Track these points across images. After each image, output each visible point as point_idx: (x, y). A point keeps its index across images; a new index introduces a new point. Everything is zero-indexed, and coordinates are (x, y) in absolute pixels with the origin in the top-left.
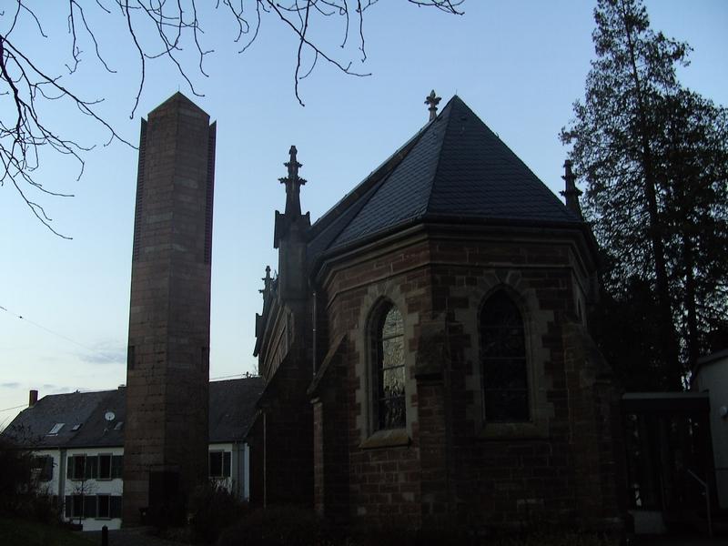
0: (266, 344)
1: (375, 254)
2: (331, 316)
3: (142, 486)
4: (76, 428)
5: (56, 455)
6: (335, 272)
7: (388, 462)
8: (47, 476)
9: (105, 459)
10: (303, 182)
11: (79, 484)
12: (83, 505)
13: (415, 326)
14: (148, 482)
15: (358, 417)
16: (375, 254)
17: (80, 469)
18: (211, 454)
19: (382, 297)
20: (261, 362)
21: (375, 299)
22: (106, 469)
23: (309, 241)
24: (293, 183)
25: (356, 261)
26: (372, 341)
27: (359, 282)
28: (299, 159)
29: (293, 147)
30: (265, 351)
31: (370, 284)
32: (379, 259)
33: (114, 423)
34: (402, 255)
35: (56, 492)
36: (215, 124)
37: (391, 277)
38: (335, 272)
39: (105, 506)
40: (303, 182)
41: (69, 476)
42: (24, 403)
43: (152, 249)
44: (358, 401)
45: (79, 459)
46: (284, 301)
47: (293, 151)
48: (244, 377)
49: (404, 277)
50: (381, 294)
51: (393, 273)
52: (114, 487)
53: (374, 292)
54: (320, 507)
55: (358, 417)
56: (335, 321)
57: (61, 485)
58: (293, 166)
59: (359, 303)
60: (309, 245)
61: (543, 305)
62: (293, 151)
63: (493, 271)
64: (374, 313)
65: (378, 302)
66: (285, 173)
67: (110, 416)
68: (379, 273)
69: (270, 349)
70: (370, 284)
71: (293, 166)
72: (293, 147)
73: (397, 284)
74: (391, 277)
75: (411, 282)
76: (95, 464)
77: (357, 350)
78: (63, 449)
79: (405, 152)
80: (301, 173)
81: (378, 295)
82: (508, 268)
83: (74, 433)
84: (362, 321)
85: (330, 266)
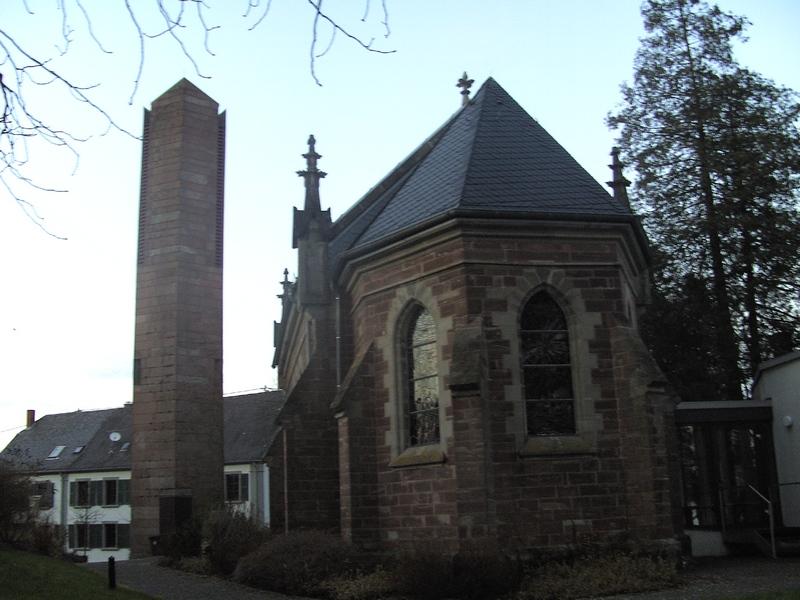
0: (285, 356)
3: (152, 512)
4: (78, 450)
5: (56, 480)
6: (360, 274)
8: (48, 504)
9: (111, 484)
10: (323, 175)
11: (83, 512)
12: (86, 535)
13: (449, 331)
15: (387, 432)
17: (83, 495)
19: (413, 300)
20: (280, 373)
21: (405, 302)
22: (112, 494)
23: (331, 240)
24: (312, 177)
29: (312, 136)
30: (284, 361)
33: (119, 444)
35: (57, 520)
36: (224, 113)
38: (360, 274)
39: (112, 535)
40: (323, 175)
41: (72, 503)
42: (22, 424)
43: (157, 252)
44: (387, 415)
45: (82, 484)
46: (305, 306)
47: (312, 141)
48: (263, 391)
49: (436, 277)
51: (424, 274)
52: (121, 514)
53: (403, 295)
56: (360, 328)
57: (62, 513)
58: (312, 157)
59: (386, 307)
60: (331, 244)
61: (591, 307)
62: (312, 141)
63: (534, 270)
66: (303, 166)
67: (115, 437)
71: (312, 157)
72: (312, 136)
78: (65, 473)
80: (321, 165)
81: (408, 298)
83: (76, 456)
84: (390, 327)
85: (354, 267)
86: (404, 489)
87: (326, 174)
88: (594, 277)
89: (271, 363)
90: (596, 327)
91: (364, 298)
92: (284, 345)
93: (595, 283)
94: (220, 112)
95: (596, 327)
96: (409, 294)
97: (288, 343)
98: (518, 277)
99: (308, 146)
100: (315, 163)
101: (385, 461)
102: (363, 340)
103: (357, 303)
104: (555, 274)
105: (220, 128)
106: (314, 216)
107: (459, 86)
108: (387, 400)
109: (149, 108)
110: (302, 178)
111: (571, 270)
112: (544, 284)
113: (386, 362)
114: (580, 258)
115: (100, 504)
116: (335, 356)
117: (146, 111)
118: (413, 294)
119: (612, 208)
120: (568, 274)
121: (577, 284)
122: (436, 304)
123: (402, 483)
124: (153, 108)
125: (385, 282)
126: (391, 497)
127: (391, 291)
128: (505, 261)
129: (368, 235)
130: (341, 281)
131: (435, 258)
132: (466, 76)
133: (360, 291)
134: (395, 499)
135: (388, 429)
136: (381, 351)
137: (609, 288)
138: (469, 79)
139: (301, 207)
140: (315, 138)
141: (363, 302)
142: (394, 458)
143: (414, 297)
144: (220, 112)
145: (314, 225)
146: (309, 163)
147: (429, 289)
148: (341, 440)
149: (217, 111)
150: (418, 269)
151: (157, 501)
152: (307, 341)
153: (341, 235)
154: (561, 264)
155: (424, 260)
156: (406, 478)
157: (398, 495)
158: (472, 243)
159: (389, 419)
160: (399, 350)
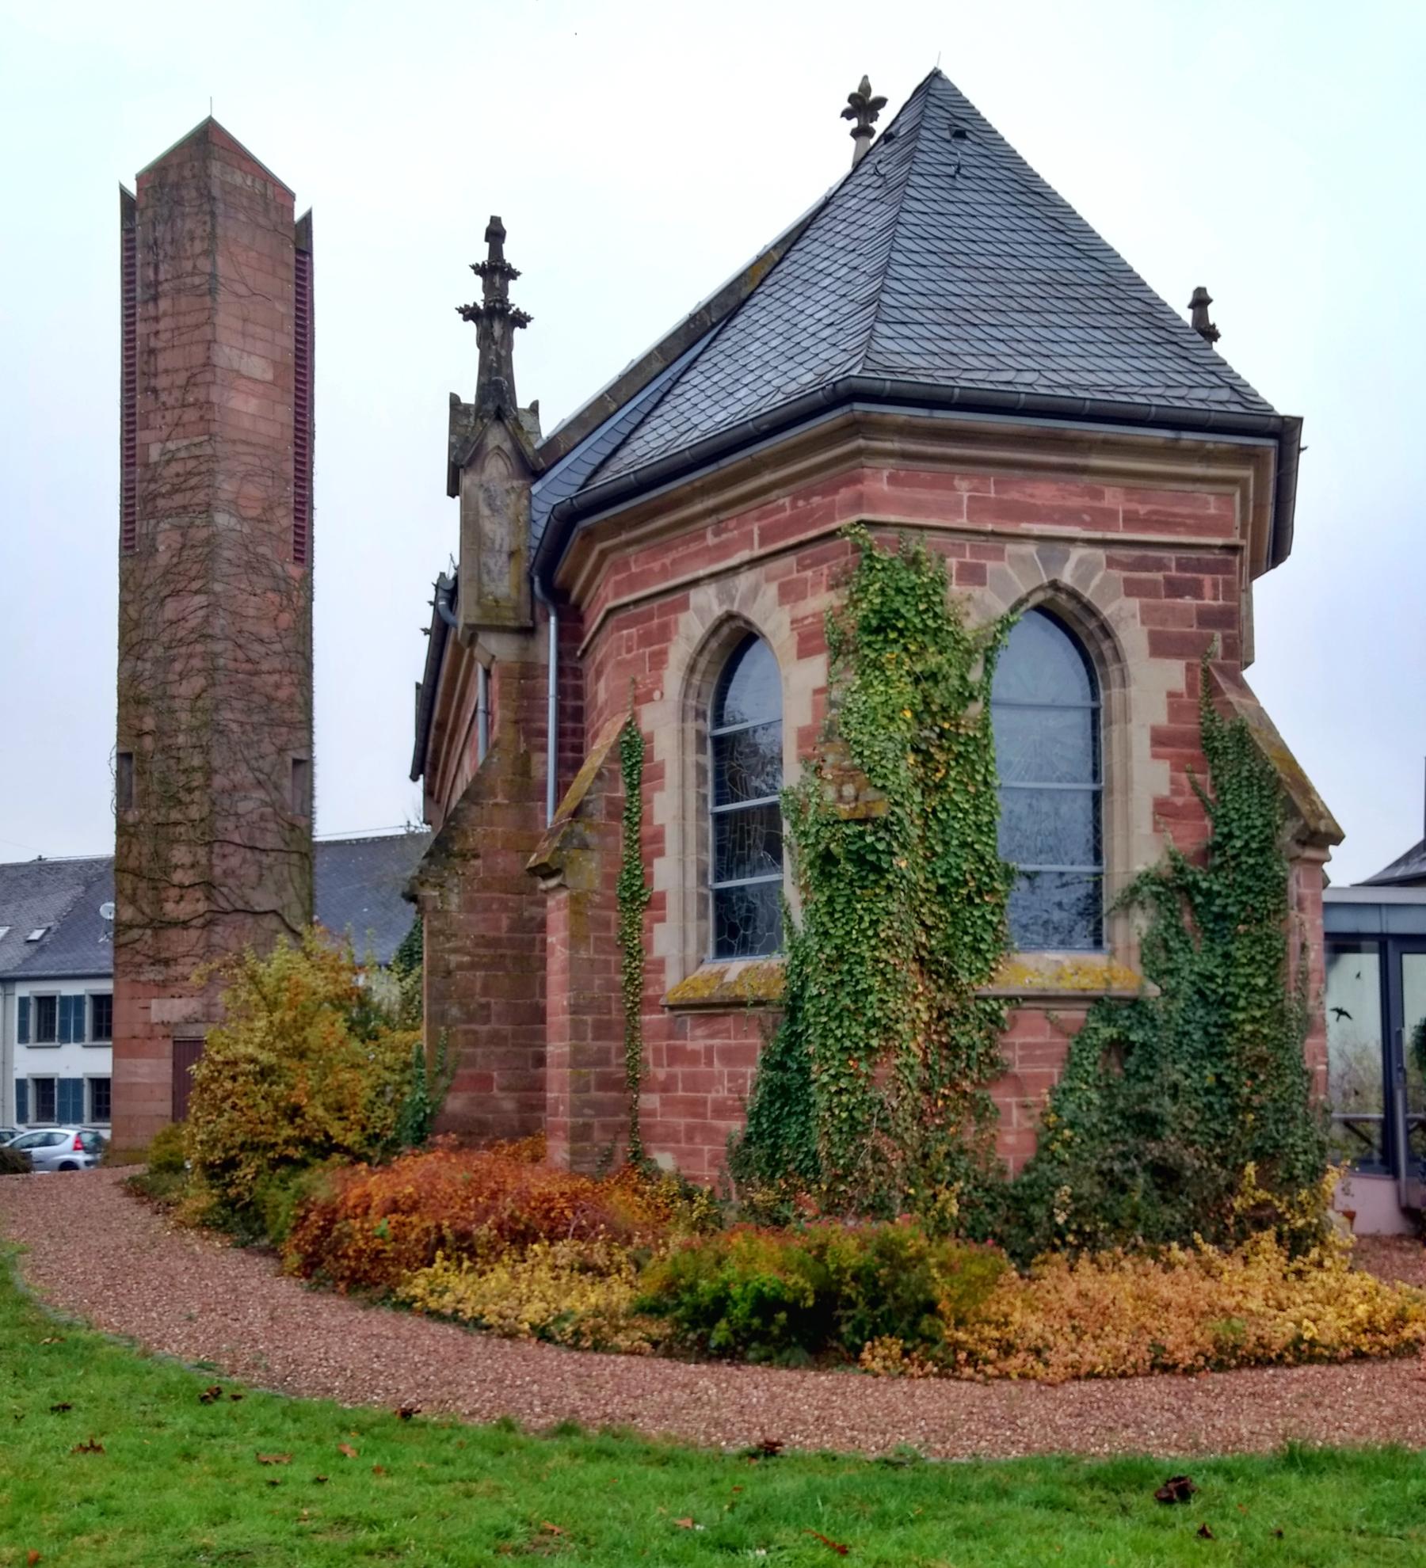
0: (437, 752)
1: (711, 502)
2: (591, 674)
4: (36, 935)
6: (603, 554)
7: (732, 1042)
10: (521, 320)
13: (818, 691)
14: (170, 1062)
15: (657, 926)
16: (711, 502)
18: (1171, 720)
19: (730, 617)
20: (429, 793)
21: (709, 622)
25: (661, 522)
26: (698, 732)
27: (666, 579)
28: (511, 253)
29: (495, 221)
30: (435, 768)
31: (695, 583)
32: (723, 516)
34: (787, 501)
36: (307, 219)
37: (754, 563)
38: (603, 554)
40: (521, 320)
44: (658, 886)
47: (495, 234)
48: (402, 832)
49: (790, 560)
50: (725, 608)
51: (758, 552)
53: (707, 604)
54: (559, 1151)
55: (657, 926)
56: (602, 684)
59: (664, 633)
60: (536, 489)
61: (1161, 646)
62: (495, 234)
63: (1030, 549)
64: (706, 656)
65: (715, 631)
66: (474, 293)
68: (724, 550)
69: (446, 765)
70: (695, 583)
72: (495, 221)
73: (769, 579)
74: (754, 563)
75: (809, 573)
76: (80, 1011)
77: (657, 758)
79: (795, 236)
80: (518, 295)
81: (718, 611)
82: (1071, 541)
83: (34, 947)
84: (673, 678)
85: (590, 535)
86: (693, 1057)
87: (529, 319)
88: (1174, 573)
89: (408, 771)
90: (1171, 695)
91: (611, 612)
92: (433, 731)
93: (1175, 589)
94: (298, 214)
95: (1171, 695)
96: (721, 603)
97: (441, 726)
98: (991, 565)
99: (485, 247)
100: (504, 290)
101: (650, 992)
102: (606, 713)
103: (594, 628)
104: (1081, 561)
105: (299, 252)
106: (500, 416)
107: (847, 114)
108: (661, 853)
109: (132, 188)
110: (471, 326)
111: (1120, 553)
112: (1054, 585)
113: (662, 764)
114: (1146, 523)
115: (79, 1037)
116: (544, 749)
117: (124, 193)
118: (732, 600)
119: (1236, 398)
120: (1111, 563)
121: (1132, 589)
122: (787, 626)
123: (690, 1045)
124: (139, 190)
125: (665, 573)
126: (661, 1073)
127: (678, 595)
128: (963, 522)
129: (615, 465)
130: (560, 576)
131: (788, 512)
132: (865, 88)
133: (606, 595)
134: (672, 1078)
135: (662, 919)
136: (650, 739)
137: (1207, 602)
138: (874, 95)
139: (469, 397)
140: (505, 224)
141: (611, 623)
142: (671, 984)
143: (735, 608)
144: (298, 214)
145: (496, 437)
146: (488, 288)
147: (772, 590)
148: (551, 939)
149: (291, 210)
150: (746, 540)
151: (168, 1047)
152: (481, 717)
153: (567, 461)
154: (1098, 535)
155: (759, 519)
156: (699, 1032)
157: (679, 1070)
158: (886, 473)
159: (662, 896)
160: (691, 736)
